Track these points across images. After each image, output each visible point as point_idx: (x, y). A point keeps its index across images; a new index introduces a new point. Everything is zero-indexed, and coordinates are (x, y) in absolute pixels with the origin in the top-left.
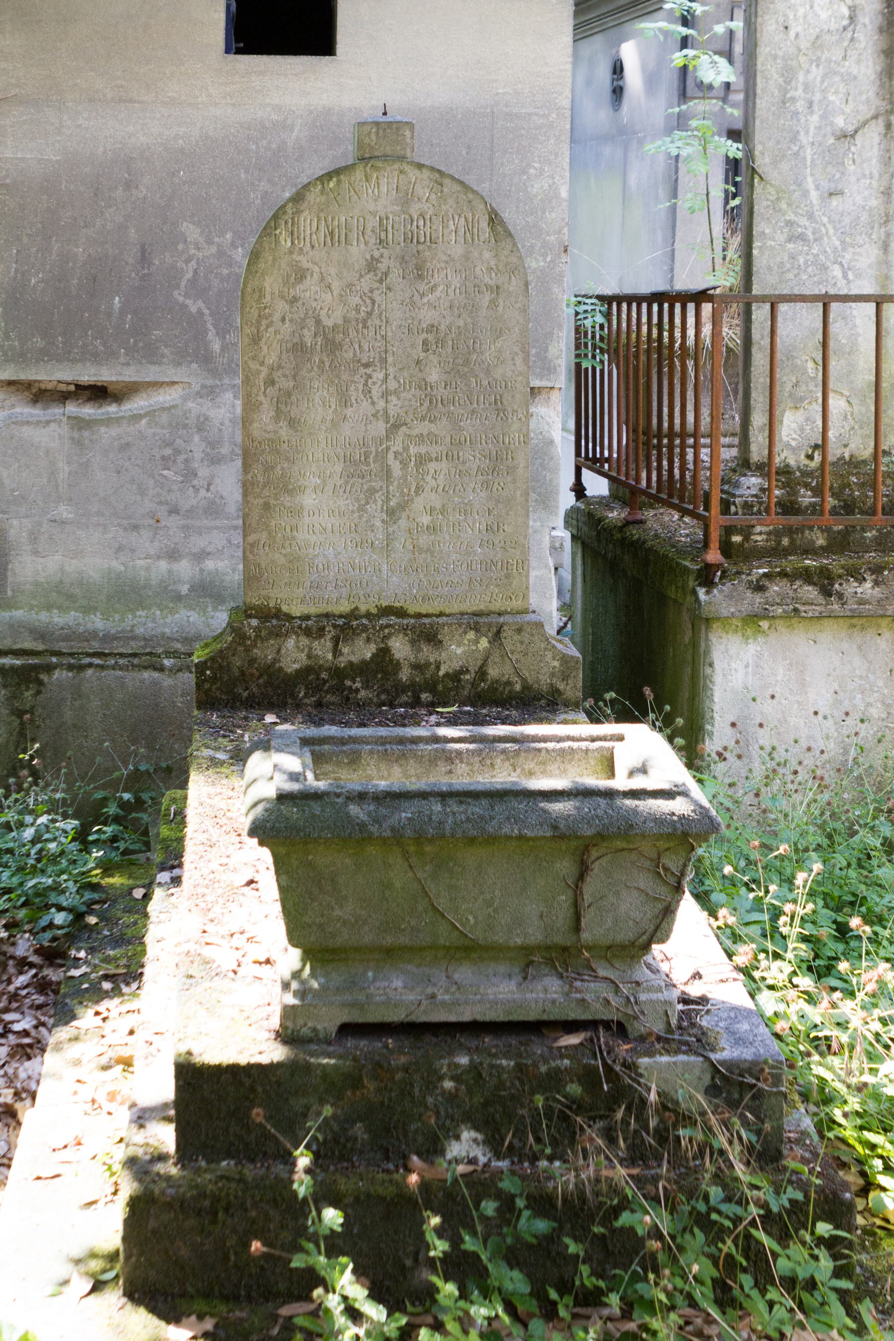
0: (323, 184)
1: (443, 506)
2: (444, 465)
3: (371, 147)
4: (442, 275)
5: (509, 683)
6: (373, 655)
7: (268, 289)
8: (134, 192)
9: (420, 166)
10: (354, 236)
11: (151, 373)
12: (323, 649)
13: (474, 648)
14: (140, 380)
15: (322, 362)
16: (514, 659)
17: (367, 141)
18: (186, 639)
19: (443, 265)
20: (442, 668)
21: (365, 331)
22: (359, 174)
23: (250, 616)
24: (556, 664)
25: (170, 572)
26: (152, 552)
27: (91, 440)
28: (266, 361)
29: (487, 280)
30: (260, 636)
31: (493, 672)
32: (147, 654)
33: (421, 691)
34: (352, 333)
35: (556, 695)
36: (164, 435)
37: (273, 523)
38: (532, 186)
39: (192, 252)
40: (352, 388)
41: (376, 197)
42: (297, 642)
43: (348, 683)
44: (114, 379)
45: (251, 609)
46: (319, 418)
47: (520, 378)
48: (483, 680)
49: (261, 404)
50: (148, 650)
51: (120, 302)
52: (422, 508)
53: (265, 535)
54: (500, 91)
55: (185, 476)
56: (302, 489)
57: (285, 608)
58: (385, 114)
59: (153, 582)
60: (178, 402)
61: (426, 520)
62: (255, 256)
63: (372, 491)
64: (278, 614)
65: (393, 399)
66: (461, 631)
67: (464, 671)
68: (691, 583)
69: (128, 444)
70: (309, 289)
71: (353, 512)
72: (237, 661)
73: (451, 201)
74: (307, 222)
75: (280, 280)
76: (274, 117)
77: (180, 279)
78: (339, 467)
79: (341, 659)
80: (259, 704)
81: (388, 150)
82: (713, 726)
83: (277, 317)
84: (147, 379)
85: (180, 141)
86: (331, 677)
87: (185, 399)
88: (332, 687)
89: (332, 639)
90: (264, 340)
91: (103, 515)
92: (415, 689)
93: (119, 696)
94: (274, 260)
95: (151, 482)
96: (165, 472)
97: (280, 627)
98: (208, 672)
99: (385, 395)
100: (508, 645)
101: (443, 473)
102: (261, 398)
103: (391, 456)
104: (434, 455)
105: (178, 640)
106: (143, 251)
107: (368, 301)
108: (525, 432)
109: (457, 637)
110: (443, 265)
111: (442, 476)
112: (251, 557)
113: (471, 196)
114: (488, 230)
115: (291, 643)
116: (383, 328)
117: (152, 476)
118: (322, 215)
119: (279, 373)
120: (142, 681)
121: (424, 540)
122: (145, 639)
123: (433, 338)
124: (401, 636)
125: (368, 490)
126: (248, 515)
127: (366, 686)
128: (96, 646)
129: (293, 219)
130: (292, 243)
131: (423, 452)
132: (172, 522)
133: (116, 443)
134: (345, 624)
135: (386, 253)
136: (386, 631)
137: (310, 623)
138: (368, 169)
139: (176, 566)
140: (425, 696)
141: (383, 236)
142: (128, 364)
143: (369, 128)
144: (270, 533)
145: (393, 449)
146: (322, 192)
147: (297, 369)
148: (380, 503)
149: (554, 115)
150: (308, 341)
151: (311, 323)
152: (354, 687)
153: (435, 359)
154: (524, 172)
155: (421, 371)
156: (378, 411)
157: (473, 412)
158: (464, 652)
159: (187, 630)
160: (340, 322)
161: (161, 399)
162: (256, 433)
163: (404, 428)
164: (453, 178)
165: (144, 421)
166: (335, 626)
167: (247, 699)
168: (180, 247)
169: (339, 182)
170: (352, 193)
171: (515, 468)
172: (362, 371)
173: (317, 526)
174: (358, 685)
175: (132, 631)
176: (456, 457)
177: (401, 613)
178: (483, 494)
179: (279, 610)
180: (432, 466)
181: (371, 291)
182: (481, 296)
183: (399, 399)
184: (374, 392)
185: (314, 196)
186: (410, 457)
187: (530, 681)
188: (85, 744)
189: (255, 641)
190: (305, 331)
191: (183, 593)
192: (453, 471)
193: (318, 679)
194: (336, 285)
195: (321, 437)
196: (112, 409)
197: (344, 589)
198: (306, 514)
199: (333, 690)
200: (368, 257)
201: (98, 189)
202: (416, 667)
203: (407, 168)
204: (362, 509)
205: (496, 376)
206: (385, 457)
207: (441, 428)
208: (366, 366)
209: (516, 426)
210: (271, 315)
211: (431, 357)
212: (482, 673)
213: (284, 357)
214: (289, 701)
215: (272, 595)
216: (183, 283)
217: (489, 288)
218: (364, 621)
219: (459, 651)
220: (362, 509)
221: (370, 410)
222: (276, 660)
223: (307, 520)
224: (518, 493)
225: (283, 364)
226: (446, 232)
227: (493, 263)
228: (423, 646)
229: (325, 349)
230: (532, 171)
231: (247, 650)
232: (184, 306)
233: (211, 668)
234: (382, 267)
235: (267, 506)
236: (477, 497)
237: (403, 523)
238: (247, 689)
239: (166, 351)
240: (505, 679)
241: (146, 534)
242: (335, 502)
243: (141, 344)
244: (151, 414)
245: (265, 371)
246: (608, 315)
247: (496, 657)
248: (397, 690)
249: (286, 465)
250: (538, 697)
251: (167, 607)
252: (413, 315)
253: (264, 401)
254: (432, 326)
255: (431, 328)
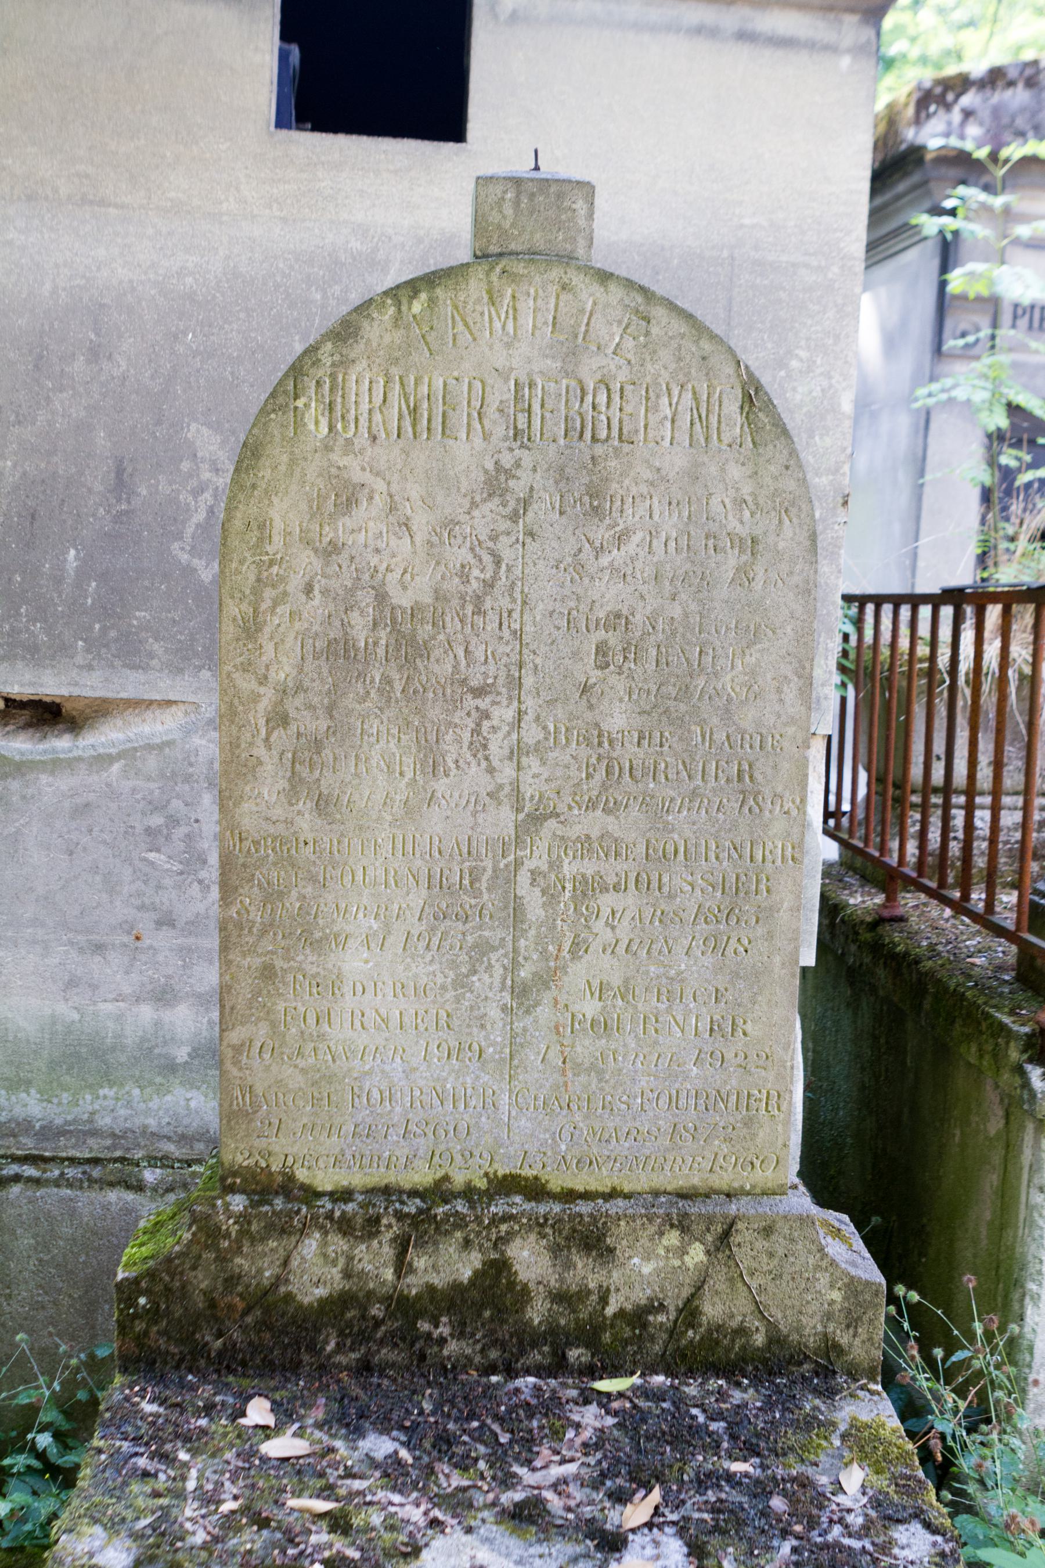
0: (398, 304)
1: (626, 981)
2: (630, 901)
3: (503, 233)
4: (642, 510)
5: (741, 1331)
6: (476, 1273)
7: (278, 525)
8: (105, 365)
9: (604, 277)
10: (460, 419)
11: (128, 684)
12: (375, 1261)
13: (677, 1263)
14: (110, 695)
15: (387, 680)
16: (754, 1285)
17: (495, 217)
18: (183, 1137)
19: (644, 489)
20: (612, 1300)
21: (479, 621)
22: (475, 287)
23: (231, 1189)
24: (836, 1295)
25: (158, 1024)
26: (127, 990)
27: (24, 797)
28: (272, 674)
29: (733, 524)
30: (248, 1232)
31: (712, 1310)
32: (116, 1160)
33: (569, 1344)
34: (452, 624)
35: (833, 1356)
36: (152, 792)
37: (281, 1006)
38: (794, 389)
39: (206, 475)
40: (448, 738)
41: (509, 339)
42: (324, 1244)
43: (424, 1326)
44: (65, 691)
45: (235, 1174)
46: (379, 797)
47: (791, 730)
48: (692, 1325)
49: (260, 763)
50: (118, 1154)
51: (77, 558)
52: (582, 985)
53: (262, 1031)
54: (747, 221)
55: (187, 863)
56: (341, 940)
57: (302, 1175)
58: (537, 168)
59: (129, 1041)
60: (177, 735)
61: (590, 1008)
62: (250, 454)
63: (483, 948)
64: (288, 1187)
65: (532, 763)
66: (652, 1229)
67: (656, 1306)
68: (1014, 1054)
69: (87, 805)
70: (364, 528)
71: (443, 987)
72: (201, 1281)
73: (665, 355)
74: (363, 383)
75: (303, 506)
76: (355, 245)
77: (184, 522)
78: (417, 899)
79: (410, 1279)
80: (244, 1364)
81: (539, 241)
82: (1040, 1285)
83: (295, 583)
84: (124, 695)
85: (189, 280)
86: (390, 1315)
87: (188, 731)
88: (392, 1334)
89: (393, 1240)
90: (267, 630)
91: (43, 925)
92: (556, 1339)
93: (66, 1230)
94: (293, 462)
95: (127, 872)
96: (152, 856)
97: (291, 1214)
98: (142, 1301)
99: (517, 753)
100: (744, 1258)
101: (629, 915)
102: (260, 751)
103: (524, 878)
104: (611, 880)
105: (169, 1139)
106: (120, 472)
107: (487, 559)
108: (795, 837)
109: (644, 1241)
110: (644, 489)
111: (625, 922)
112: (235, 1072)
113: (706, 345)
114: (739, 419)
115: (311, 1245)
116: (516, 615)
117: (128, 860)
118: (395, 371)
119: (298, 701)
120: (106, 1207)
121: (585, 1048)
122: (113, 1135)
123: (619, 642)
124: (533, 1237)
125: (475, 946)
126: (229, 988)
127: (460, 1333)
128: (28, 1145)
129: (333, 376)
130: (331, 428)
131: (589, 873)
132: (163, 940)
133: (67, 804)
134: (420, 1211)
135: (527, 458)
136: (504, 1227)
137: (350, 1207)
138: (494, 278)
139: (168, 1016)
140: (576, 1354)
141: (522, 424)
142: (90, 668)
143: (499, 189)
144: (273, 1025)
145: (529, 864)
146: (397, 320)
147: (335, 694)
148: (498, 971)
149: (835, 269)
150: (360, 634)
151: (366, 598)
152: (436, 1334)
153: (620, 684)
154: (781, 364)
155: (591, 707)
156: (501, 787)
157: (694, 793)
158: (657, 1272)
159: (186, 1121)
160: (428, 599)
161: (146, 729)
162: (247, 823)
163: (552, 823)
164: (672, 306)
165: (116, 767)
166: (400, 1216)
167: (220, 1354)
168: (185, 466)
169: (432, 301)
170: (460, 327)
171: (772, 910)
172: (470, 702)
173: (371, 1014)
174: (444, 1330)
175: (91, 1121)
176: (655, 884)
177: (535, 1190)
178: (708, 960)
179: (291, 1178)
180: (607, 901)
181: (494, 538)
182: (720, 557)
183: (543, 763)
184: (493, 748)
185: (378, 330)
186: (562, 881)
187: (784, 1329)
188: (7, 1309)
189: (238, 1241)
190: (355, 616)
191: (179, 1060)
192: (648, 913)
193: (363, 1317)
194: (421, 522)
195: (383, 836)
196: (61, 743)
197: (422, 1140)
198: (347, 989)
199: (391, 1340)
200: (490, 466)
201: (41, 357)
202: (560, 1297)
203: (577, 279)
204: (461, 983)
205: (743, 724)
206: (511, 880)
207: (629, 826)
208: (479, 692)
209: (778, 827)
210: (283, 579)
211: (613, 679)
212: (690, 1312)
213: (309, 666)
214: (306, 1358)
215: (276, 1148)
216: (189, 530)
217: (737, 541)
218: (461, 1206)
219: (647, 1269)
220: (461, 983)
221: (485, 784)
222: (278, 1281)
223: (349, 1002)
224: (777, 959)
225: (307, 683)
226: (653, 419)
227: (746, 490)
228: (576, 1258)
229: (391, 653)
230: (794, 364)
231: (222, 1259)
232: (189, 571)
233: (147, 1292)
234: (518, 487)
235: (268, 973)
236: (695, 967)
237: (544, 1013)
238: (219, 1335)
239: (157, 647)
240: (734, 1324)
241: (116, 959)
242: (407, 968)
243: (113, 634)
244: (128, 754)
245: (268, 696)
246: (858, 622)
247: (718, 1281)
248: (521, 1342)
249: (309, 890)
250: (797, 1357)
251: (151, 1083)
252: (580, 591)
253: (266, 759)
254: (618, 616)
255: (617, 620)
